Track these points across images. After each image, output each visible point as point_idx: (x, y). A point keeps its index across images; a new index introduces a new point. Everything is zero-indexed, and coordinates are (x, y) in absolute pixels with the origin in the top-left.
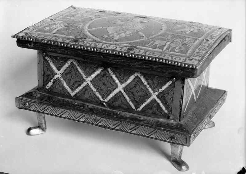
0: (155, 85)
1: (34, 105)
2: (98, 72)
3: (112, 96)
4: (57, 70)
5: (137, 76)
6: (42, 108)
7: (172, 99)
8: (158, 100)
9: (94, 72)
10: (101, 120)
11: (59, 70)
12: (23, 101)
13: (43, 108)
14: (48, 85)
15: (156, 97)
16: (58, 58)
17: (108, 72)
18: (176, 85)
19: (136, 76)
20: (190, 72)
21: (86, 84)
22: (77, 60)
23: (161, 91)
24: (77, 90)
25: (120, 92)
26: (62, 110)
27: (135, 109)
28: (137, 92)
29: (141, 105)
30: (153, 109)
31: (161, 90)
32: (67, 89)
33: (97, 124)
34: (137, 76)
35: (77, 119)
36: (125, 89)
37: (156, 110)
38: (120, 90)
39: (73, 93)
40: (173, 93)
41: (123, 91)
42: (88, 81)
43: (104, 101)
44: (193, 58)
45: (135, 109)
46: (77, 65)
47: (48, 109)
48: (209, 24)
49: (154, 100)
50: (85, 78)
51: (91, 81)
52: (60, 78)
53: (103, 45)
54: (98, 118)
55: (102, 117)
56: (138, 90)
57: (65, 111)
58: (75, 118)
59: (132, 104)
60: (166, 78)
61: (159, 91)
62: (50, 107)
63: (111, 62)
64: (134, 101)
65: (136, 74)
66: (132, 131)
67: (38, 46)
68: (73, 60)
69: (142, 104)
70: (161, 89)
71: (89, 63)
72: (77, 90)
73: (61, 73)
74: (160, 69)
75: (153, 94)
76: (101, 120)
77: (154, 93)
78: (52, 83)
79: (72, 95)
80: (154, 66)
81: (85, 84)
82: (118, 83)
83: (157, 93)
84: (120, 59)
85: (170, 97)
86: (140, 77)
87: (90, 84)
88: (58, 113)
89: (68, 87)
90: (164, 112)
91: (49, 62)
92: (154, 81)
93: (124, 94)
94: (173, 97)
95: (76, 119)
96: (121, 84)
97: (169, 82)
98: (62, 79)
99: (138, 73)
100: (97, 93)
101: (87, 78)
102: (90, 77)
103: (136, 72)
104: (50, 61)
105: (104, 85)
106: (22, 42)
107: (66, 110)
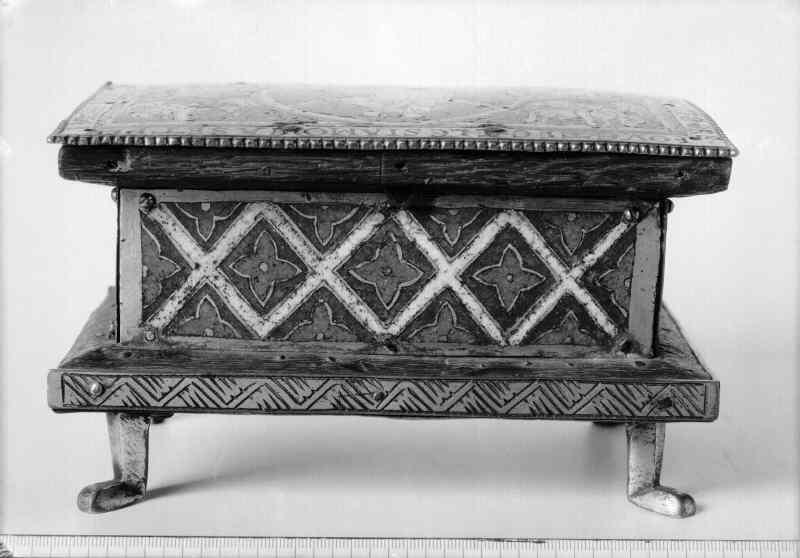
0: (572, 244)
1: (641, 406)
2: (363, 232)
3: (418, 309)
4: (202, 253)
5: (508, 225)
6: (536, 399)
7: (627, 284)
8: (583, 296)
9: (345, 231)
10: (396, 391)
11: (207, 247)
12: (675, 414)
13: (167, 390)
14: (162, 314)
15: (576, 285)
16: (206, 207)
17: (398, 226)
18: (640, 234)
19: (503, 224)
20: (712, 172)
21: (318, 282)
22: (280, 204)
23: (593, 263)
24: (283, 312)
25: (448, 290)
26: (243, 382)
27: (500, 338)
28: (509, 277)
29: (523, 321)
30: (566, 329)
31: (592, 260)
32: (241, 312)
33: (307, 409)
34: (508, 225)
35: (305, 406)
36: (466, 278)
37: (574, 329)
38: (444, 284)
39: (267, 324)
40: (633, 264)
41: (456, 286)
42: (325, 271)
43: (384, 331)
44: (406, 161)
45: (500, 338)
46: (278, 221)
47: (186, 389)
48: (246, 79)
49: (568, 301)
50: (314, 260)
51: (343, 271)
52: (212, 279)
53: (379, 130)
54: (387, 386)
55: (400, 381)
56: (512, 271)
57: (254, 387)
58: (296, 401)
59: (490, 322)
60: (607, 216)
61: (583, 262)
62: (266, 384)
63: (434, 181)
64: (497, 313)
65: (502, 220)
66: (68, 384)
67: (147, 164)
68: (265, 205)
69: (527, 317)
70: (590, 256)
71: (325, 207)
72: (283, 312)
73: (219, 262)
74: (608, 178)
75: (564, 275)
76: (396, 391)
77: (567, 272)
78: (180, 302)
79: (260, 334)
80: (588, 173)
81: (312, 283)
82: (436, 260)
83: (577, 272)
84: (463, 169)
85: (622, 277)
86: (517, 227)
87: (331, 283)
88: (227, 399)
89: (246, 307)
90: (604, 332)
91: (168, 228)
92: (567, 233)
93: (460, 296)
94: (631, 276)
95: (298, 407)
96: (450, 262)
97: (616, 228)
98: (220, 282)
99: (509, 214)
100: (362, 307)
101: (320, 259)
102: (333, 256)
103: (500, 211)
104: (171, 223)
105: (381, 274)
106: (85, 158)
107: (260, 382)
